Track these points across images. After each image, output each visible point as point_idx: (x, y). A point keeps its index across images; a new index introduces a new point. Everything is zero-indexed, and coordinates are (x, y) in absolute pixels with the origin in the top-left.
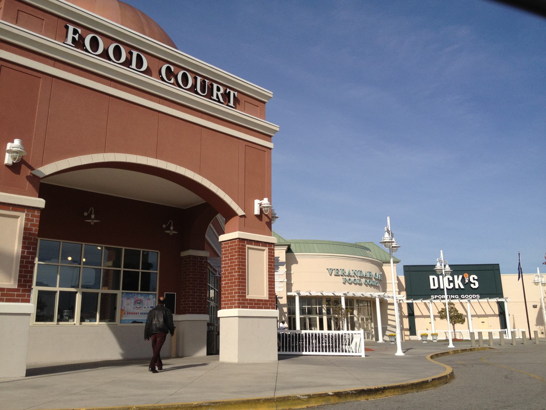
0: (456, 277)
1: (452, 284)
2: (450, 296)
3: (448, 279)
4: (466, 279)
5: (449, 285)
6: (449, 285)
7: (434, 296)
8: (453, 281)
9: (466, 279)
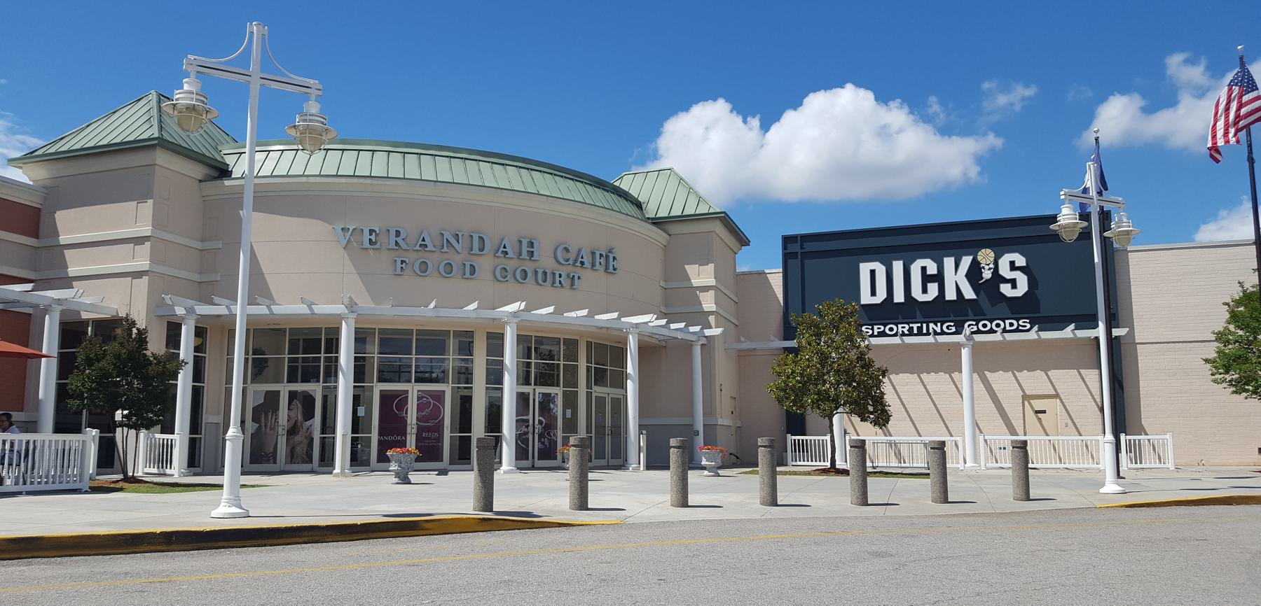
0: (949, 262)
1: (933, 289)
2: (924, 325)
3: (924, 269)
4: (987, 267)
5: (925, 291)
6: (925, 291)
7: (872, 329)
8: (939, 278)
9: (987, 267)
